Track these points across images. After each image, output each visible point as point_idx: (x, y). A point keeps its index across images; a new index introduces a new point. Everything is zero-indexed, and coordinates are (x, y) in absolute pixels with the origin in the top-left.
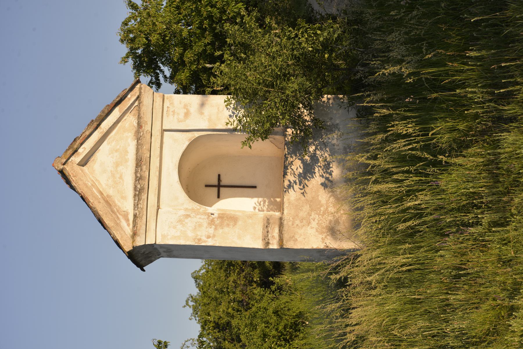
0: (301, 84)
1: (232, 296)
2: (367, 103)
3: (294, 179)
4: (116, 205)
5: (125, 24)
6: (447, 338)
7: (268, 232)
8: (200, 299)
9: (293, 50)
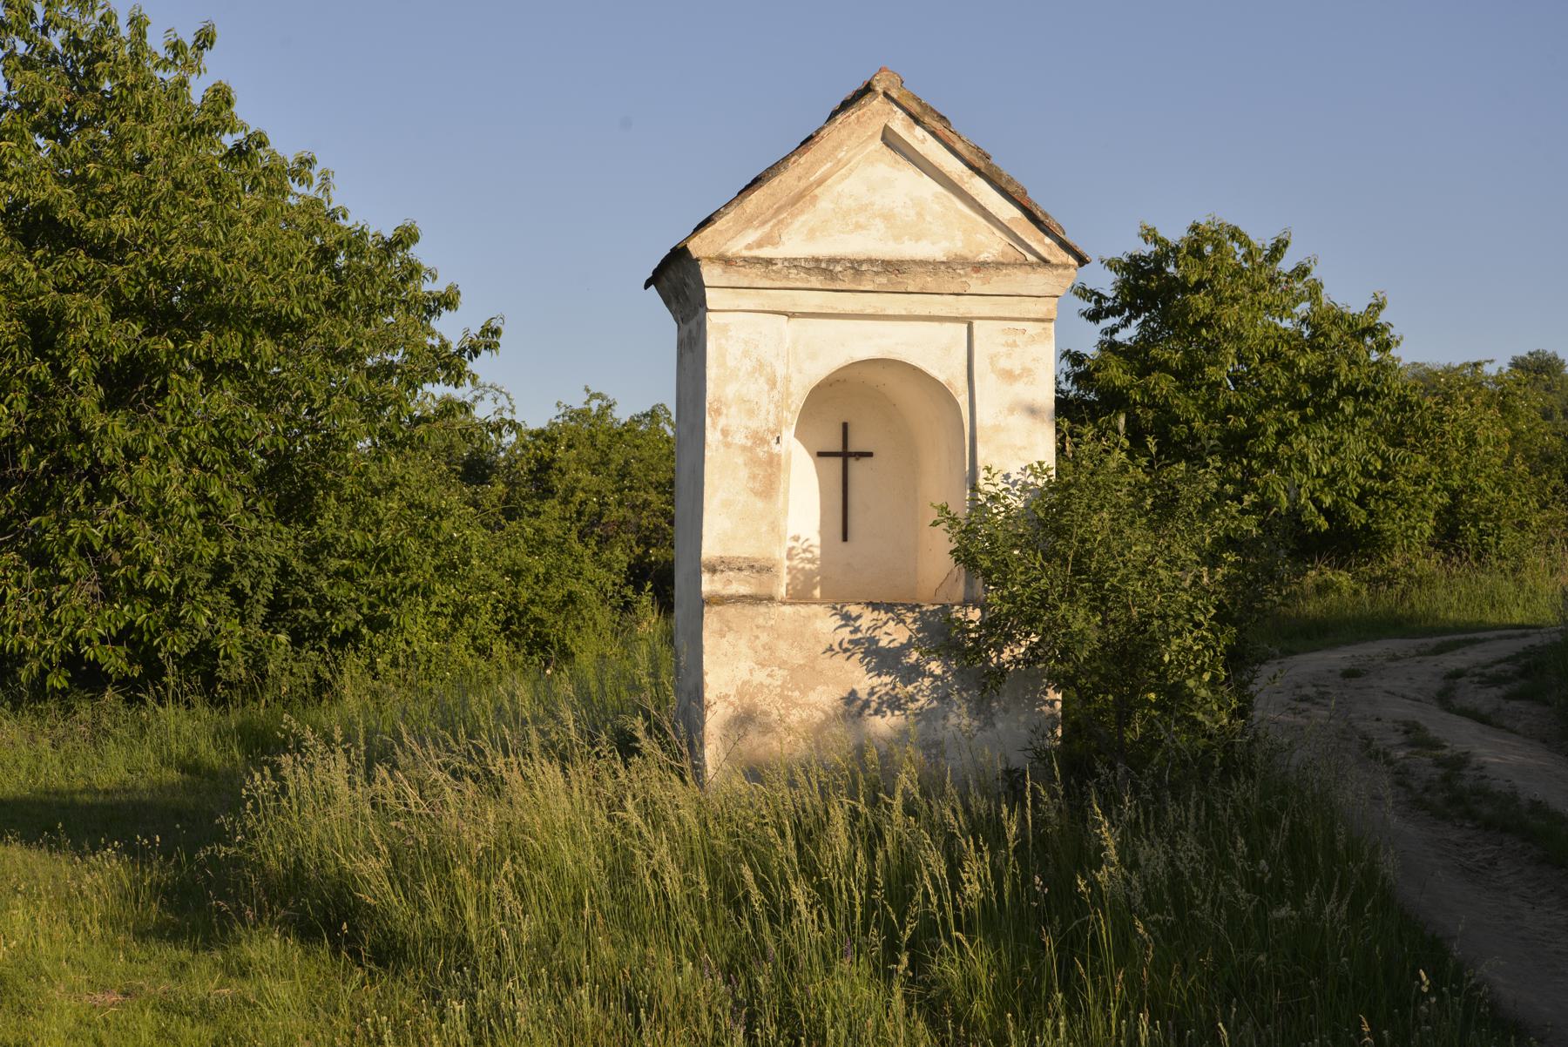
0: (1082, 637)
1: (612, 499)
2: (1033, 788)
3: (864, 628)
4: (794, 216)
5: (1235, 234)
6: (494, 983)
7: (740, 569)
8: (605, 427)
9: (1163, 617)
